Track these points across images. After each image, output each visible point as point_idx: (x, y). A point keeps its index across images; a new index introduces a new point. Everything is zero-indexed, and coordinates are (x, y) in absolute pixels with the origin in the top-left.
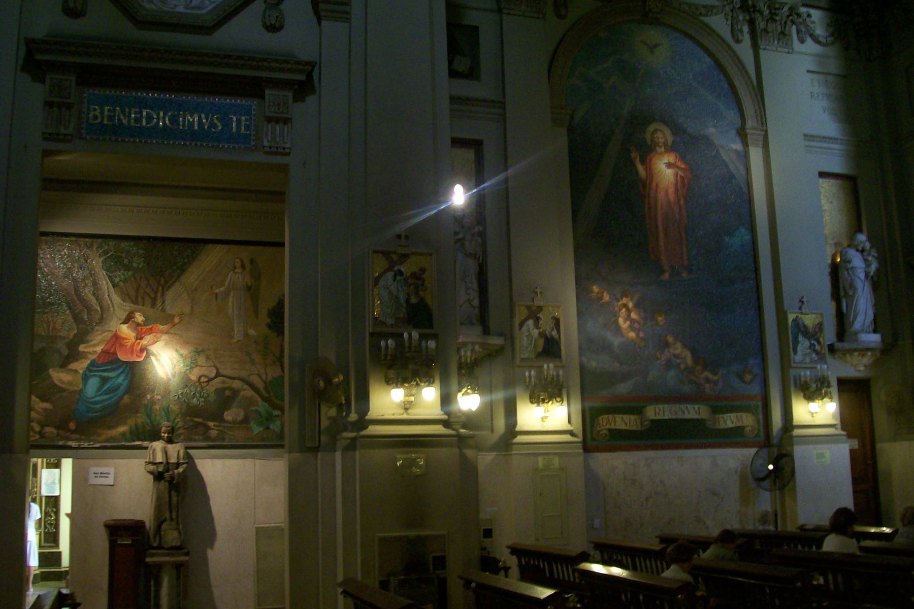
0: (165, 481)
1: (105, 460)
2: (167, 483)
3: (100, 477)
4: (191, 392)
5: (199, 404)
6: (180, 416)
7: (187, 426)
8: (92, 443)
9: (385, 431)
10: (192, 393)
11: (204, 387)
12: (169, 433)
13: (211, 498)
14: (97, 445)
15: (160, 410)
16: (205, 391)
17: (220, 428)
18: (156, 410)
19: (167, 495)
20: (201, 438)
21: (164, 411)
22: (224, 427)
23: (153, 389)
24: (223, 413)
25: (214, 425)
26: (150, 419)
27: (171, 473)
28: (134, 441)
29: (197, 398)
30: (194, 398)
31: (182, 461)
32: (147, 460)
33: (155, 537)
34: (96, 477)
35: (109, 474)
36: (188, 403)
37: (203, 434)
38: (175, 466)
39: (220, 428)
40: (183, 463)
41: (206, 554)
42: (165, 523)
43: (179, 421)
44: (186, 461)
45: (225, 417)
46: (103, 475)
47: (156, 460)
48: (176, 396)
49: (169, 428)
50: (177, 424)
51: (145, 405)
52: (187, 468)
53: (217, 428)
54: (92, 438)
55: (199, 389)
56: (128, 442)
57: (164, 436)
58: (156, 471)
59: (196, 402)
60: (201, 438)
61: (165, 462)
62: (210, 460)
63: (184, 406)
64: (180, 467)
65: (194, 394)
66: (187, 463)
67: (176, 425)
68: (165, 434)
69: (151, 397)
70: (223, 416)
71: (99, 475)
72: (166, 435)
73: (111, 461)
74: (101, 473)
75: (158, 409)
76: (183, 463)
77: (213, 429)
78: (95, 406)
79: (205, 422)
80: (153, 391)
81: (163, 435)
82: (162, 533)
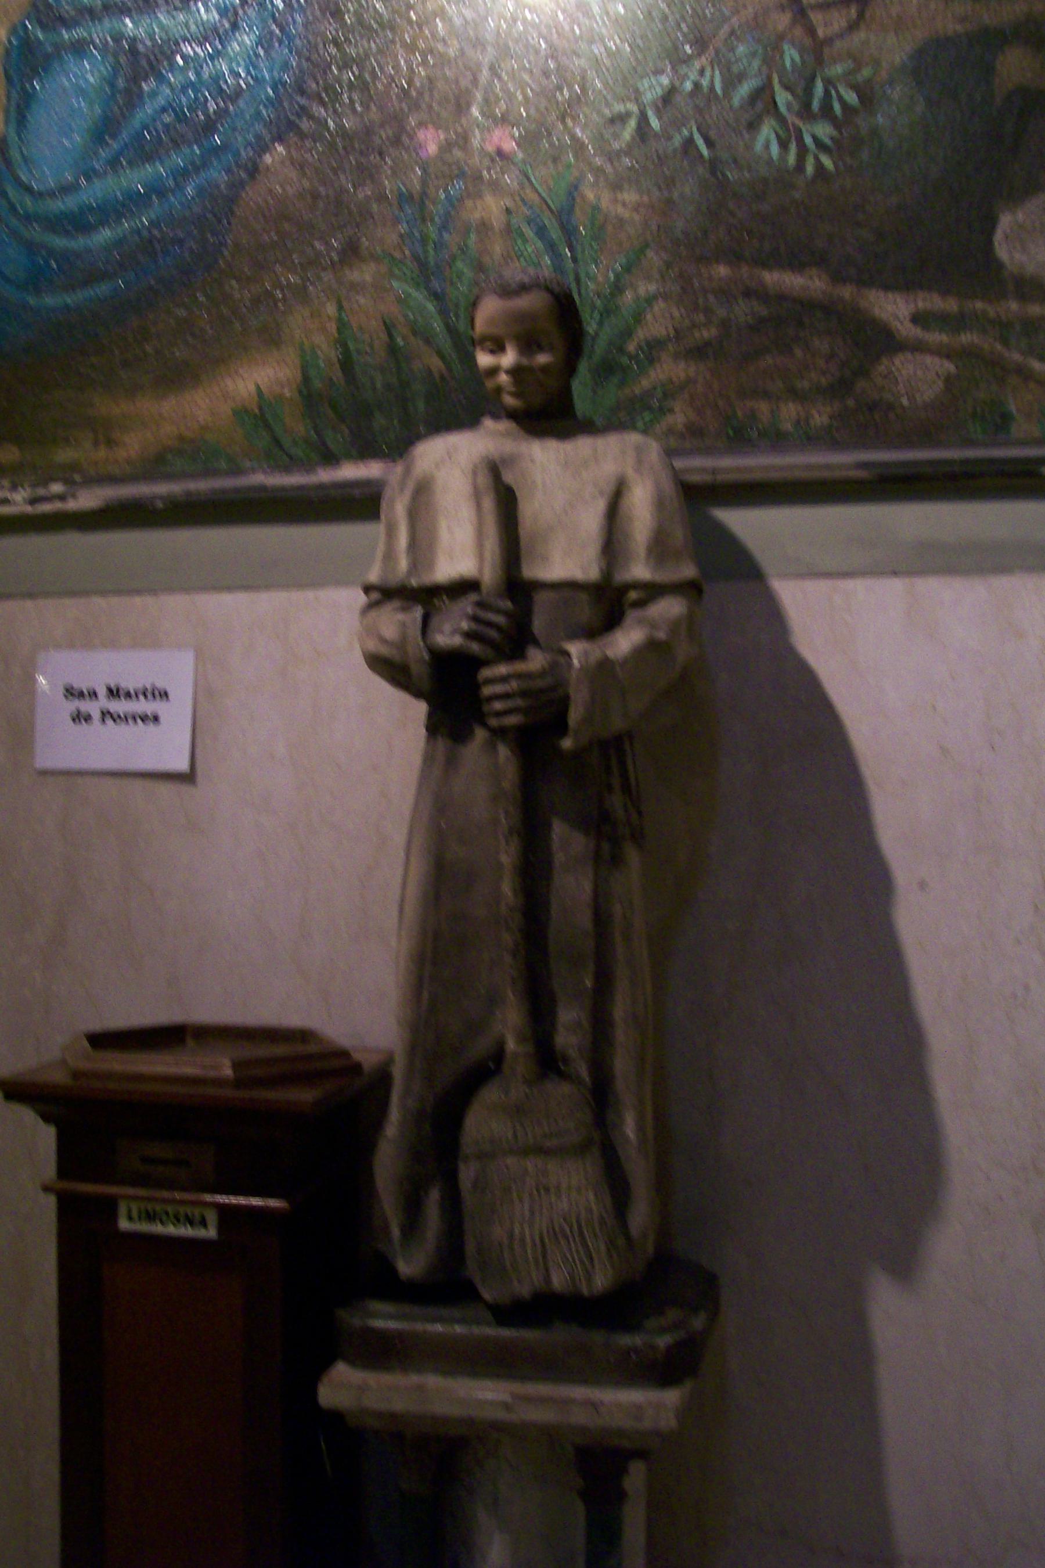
0: (499, 733)
1: (138, 600)
2: (503, 751)
3: (105, 714)
4: (731, 81)
5: (800, 167)
6: (654, 258)
7: (708, 334)
8: (57, 488)
9: (404, 885)
10: (744, 89)
11: (829, 41)
12: (528, 344)
13: (902, 876)
14: (87, 500)
15: (509, 230)
16: (838, 69)
17: (966, 338)
18: (484, 227)
19: (508, 856)
20: (820, 417)
21: (541, 232)
22: (1003, 328)
23: (464, 83)
24: (990, 223)
25: (917, 319)
26: (437, 297)
27: (536, 660)
28: (331, 459)
29: (782, 120)
30: (753, 126)
31: (640, 571)
32: (374, 576)
33: (413, 1208)
34: (85, 718)
35: (164, 695)
36: (714, 165)
37: (840, 388)
38: (585, 611)
39: (966, 338)
40: (653, 591)
41: (859, 1319)
42: (490, 1094)
43: (650, 300)
44: (688, 571)
45: (1002, 252)
46: (119, 706)
47: (431, 565)
48: (621, 119)
49: (524, 302)
50: (638, 317)
51: (405, 198)
52: (690, 624)
53: (937, 337)
54: (64, 455)
55: (791, 55)
56: (292, 463)
57: (493, 371)
58: (417, 652)
59: (775, 149)
60: (820, 417)
61: (489, 576)
62: (896, 586)
63: (687, 188)
64: (631, 616)
65: (755, 96)
66: (691, 589)
67: (627, 333)
68: (498, 347)
69: (447, 147)
70: (990, 242)
71: (92, 708)
72: (509, 358)
73: (175, 603)
74: (113, 693)
75: (497, 220)
76: (653, 591)
77: (918, 347)
78: (78, 243)
79: (846, 292)
80: (461, 105)
81: (484, 360)
82: (467, 1174)
